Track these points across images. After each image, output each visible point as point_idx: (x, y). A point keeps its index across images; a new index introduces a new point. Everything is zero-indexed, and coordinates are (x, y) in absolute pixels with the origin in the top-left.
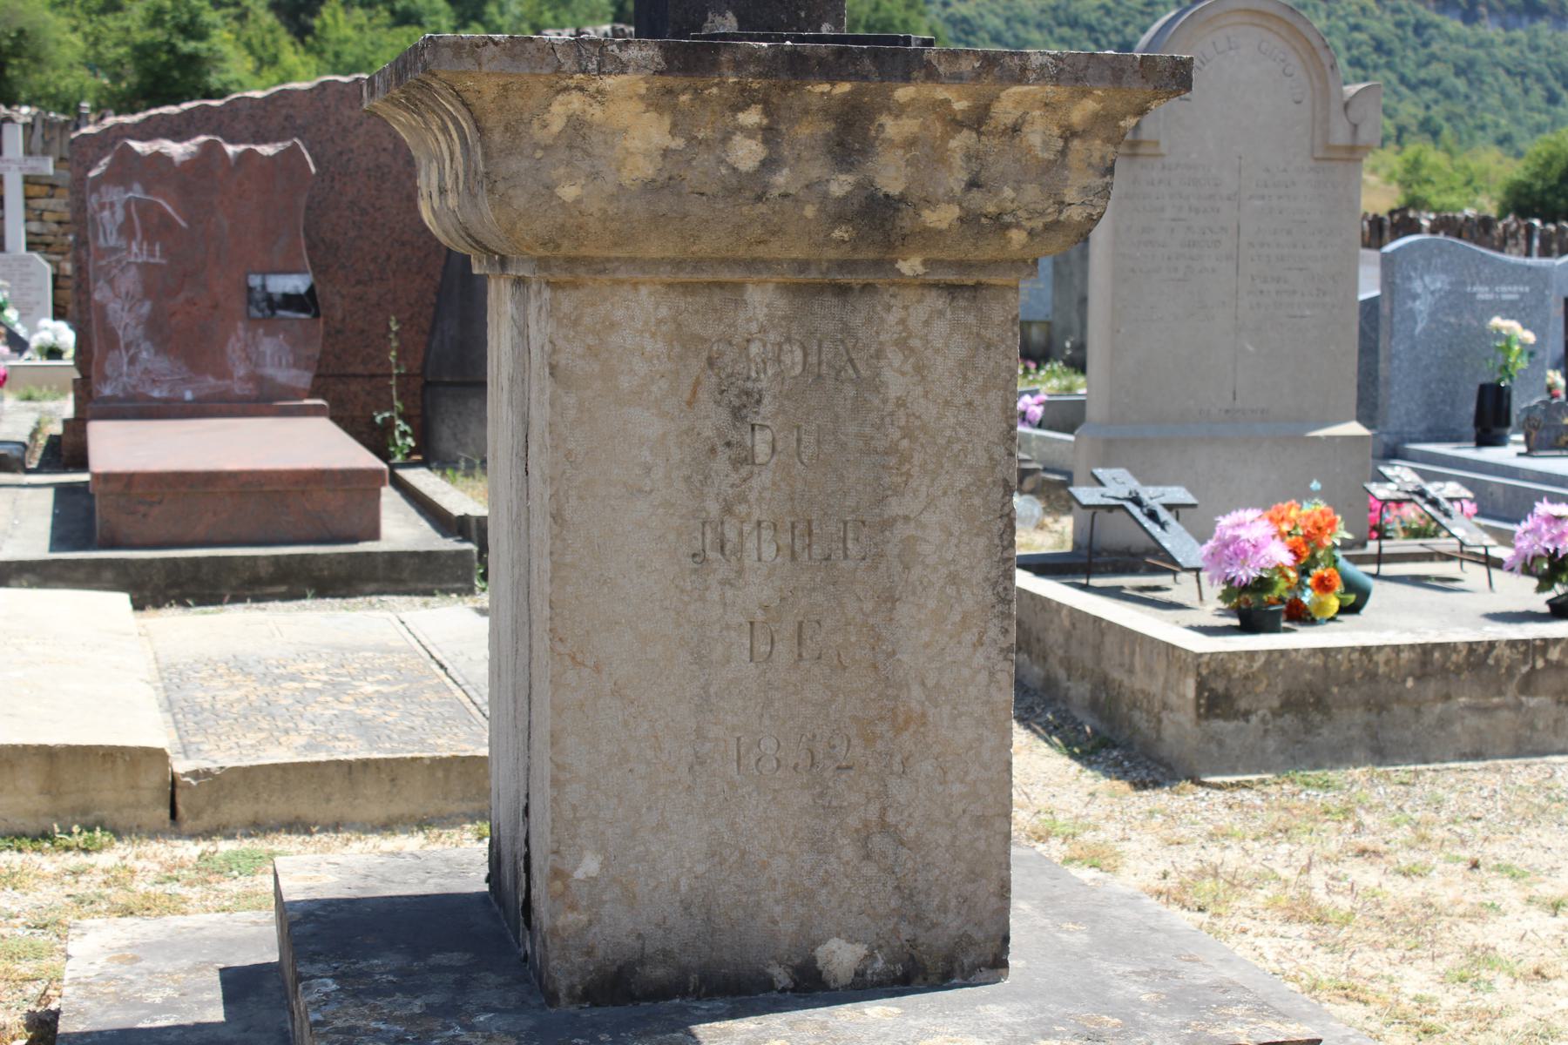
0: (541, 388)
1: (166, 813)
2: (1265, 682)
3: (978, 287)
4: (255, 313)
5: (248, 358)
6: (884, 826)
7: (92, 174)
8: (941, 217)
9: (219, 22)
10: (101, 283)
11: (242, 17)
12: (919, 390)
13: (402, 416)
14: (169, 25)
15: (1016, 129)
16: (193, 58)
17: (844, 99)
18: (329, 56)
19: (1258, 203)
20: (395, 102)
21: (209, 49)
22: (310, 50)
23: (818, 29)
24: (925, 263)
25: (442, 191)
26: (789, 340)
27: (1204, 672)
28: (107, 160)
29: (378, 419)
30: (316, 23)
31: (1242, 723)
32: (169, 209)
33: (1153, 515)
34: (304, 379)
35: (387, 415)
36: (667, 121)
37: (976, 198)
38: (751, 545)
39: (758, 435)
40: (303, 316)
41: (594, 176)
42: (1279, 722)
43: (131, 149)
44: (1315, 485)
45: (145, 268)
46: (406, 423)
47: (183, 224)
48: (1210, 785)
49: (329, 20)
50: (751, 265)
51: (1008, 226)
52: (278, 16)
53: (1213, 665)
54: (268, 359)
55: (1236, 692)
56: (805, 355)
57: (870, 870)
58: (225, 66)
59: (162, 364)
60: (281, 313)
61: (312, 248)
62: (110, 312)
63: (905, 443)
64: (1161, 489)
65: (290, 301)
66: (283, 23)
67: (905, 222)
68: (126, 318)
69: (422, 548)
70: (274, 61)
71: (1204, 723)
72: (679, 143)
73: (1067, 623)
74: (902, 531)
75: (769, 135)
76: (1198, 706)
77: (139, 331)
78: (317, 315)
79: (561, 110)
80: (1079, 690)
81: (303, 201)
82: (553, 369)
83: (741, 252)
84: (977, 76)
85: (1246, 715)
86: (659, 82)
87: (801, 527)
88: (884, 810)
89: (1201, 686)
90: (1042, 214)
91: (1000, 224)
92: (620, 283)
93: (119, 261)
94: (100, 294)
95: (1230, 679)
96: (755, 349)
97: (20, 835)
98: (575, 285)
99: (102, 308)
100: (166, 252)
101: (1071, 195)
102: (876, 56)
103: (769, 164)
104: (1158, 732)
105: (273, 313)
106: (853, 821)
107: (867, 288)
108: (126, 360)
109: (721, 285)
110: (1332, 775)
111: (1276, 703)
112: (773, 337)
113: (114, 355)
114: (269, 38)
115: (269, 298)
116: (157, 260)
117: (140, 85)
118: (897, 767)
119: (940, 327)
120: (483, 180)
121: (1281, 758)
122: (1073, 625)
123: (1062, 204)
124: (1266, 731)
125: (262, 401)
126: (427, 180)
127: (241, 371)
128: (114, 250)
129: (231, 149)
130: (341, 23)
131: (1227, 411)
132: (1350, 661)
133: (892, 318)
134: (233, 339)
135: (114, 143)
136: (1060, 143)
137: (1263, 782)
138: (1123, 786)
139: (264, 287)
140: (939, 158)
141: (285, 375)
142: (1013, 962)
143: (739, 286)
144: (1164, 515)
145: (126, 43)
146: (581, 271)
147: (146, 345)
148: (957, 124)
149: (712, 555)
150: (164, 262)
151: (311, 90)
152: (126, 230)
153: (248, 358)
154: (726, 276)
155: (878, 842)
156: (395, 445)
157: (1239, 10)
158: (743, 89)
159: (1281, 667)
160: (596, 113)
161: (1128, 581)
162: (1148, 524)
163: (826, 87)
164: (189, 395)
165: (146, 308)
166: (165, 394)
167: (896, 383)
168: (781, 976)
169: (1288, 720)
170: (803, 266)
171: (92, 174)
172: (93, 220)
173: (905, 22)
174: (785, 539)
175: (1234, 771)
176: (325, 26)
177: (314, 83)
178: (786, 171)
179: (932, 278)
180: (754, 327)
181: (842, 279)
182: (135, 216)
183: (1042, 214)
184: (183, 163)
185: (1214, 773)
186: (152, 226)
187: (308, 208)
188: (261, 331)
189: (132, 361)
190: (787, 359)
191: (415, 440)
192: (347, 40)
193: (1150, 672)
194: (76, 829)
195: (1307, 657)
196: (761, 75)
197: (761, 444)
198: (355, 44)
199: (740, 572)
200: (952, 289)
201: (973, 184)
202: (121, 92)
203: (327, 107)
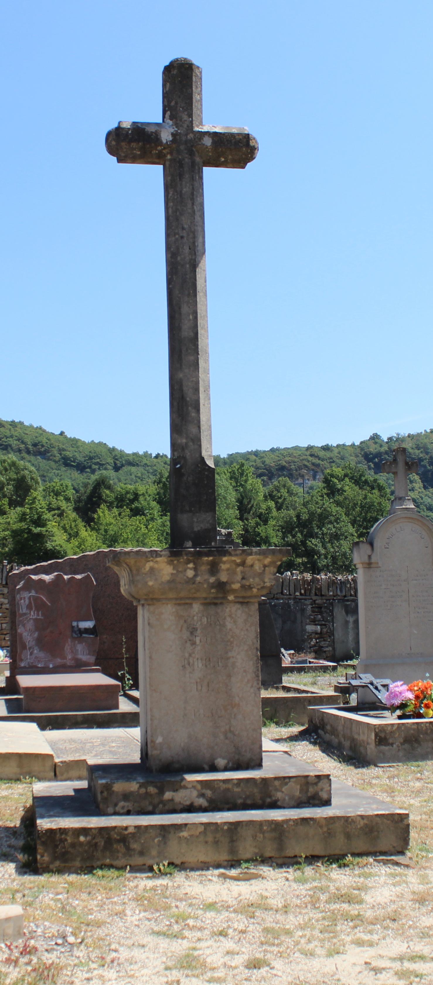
0: (147, 627)
1: (53, 774)
2: (398, 734)
3: (248, 602)
4: (75, 635)
5: (72, 652)
6: (230, 731)
7: (17, 587)
8: (236, 586)
9: (51, 518)
10: (20, 626)
11: (61, 515)
12: (235, 627)
13: (128, 673)
14: (28, 520)
15: (252, 566)
16: (40, 536)
17: (211, 561)
18: (102, 531)
19: (415, 582)
20: (112, 564)
21: (47, 531)
22: (93, 529)
23: (211, 544)
24: (235, 597)
25: (125, 585)
26: (203, 616)
27: (377, 730)
28: (22, 582)
29: (119, 674)
30: (96, 516)
31: (391, 747)
32: (44, 599)
33: (376, 688)
34: (92, 659)
35: (122, 672)
36: (172, 567)
37: (244, 582)
38: (196, 663)
39: (197, 638)
40: (91, 636)
41: (156, 580)
42: (403, 747)
43: (31, 578)
44: (427, 675)
45: (36, 620)
46: (129, 675)
47: (49, 604)
48: (380, 767)
49: (101, 514)
50: (194, 599)
51: (252, 588)
52: (78, 514)
53: (380, 728)
54: (79, 652)
55: (388, 737)
56: (207, 619)
57: (227, 741)
58: (54, 538)
59: (42, 655)
60: (84, 635)
61: (95, 612)
62: (24, 636)
63: (232, 639)
64: (382, 680)
65: (87, 631)
66: (80, 517)
67: (228, 587)
68: (29, 638)
69: (133, 711)
70: (77, 535)
71: (378, 747)
72: (175, 572)
73: (343, 722)
74: (232, 660)
75: (195, 569)
76: (376, 741)
77: (34, 643)
78: (97, 636)
79: (148, 565)
80: (347, 744)
81: (91, 595)
82: (149, 624)
83: (191, 596)
84: (241, 554)
85: (392, 744)
86: (169, 559)
87: (208, 659)
88: (230, 727)
89: (376, 735)
90: (260, 585)
91: (250, 587)
92: (164, 604)
93: (27, 618)
94: (20, 630)
95: (386, 733)
96: (195, 618)
97: (11, 779)
98: (153, 604)
99: (21, 635)
100: (42, 615)
101: (266, 580)
102: (217, 551)
103: (196, 576)
104: (366, 753)
105: (81, 635)
106: (223, 730)
107: (221, 603)
108: (29, 653)
109: (187, 604)
110: (420, 763)
111: (402, 740)
112: (200, 615)
113: (25, 652)
114: (73, 524)
115: (80, 630)
116: (40, 617)
117: (14, 549)
118: (233, 716)
119: (239, 612)
120: (132, 582)
121: (404, 758)
122: (345, 723)
123: (264, 582)
124: (399, 750)
125: (78, 667)
126: (122, 583)
127: (69, 657)
128: (25, 614)
129: (66, 577)
130: (107, 516)
131: (408, 654)
132: (426, 726)
133: (227, 610)
134: (67, 645)
135: (24, 577)
136: (263, 569)
137: (398, 765)
138: (352, 768)
139: (78, 626)
140: (234, 573)
141: (85, 658)
142: (263, 764)
143: (191, 604)
144: (380, 688)
145: (8, 530)
146: (155, 601)
147: (36, 648)
148: (238, 565)
149: (187, 666)
150: (42, 618)
151: (94, 555)
152: (29, 607)
153: (72, 652)
154: (187, 601)
155: (229, 735)
156: (125, 683)
157: (403, 518)
158: (188, 559)
159: (403, 729)
160: (156, 566)
161: (372, 713)
162: (374, 691)
163: (206, 558)
164: (51, 666)
165: (36, 635)
166: (42, 666)
167: (229, 624)
168: (206, 767)
169: (406, 746)
170: (205, 598)
171: (17, 587)
172: (18, 604)
173: (380, 504)
174: (204, 662)
175: (388, 762)
176: (99, 517)
177: (95, 552)
178: (199, 577)
179: (237, 600)
180: (195, 613)
181: (216, 601)
182: (32, 602)
183: (260, 585)
184: (49, 582)
185: (382, 763)
186: (38, 605)
187: (93, 597)
188: (76, 642)
189: (31, 654)
190: (203, 620)
191: (133, 681)
192: (111, 524)
193: (363, 733)
194: (27, 777)
195: (411, 726)
196: (191, 557)
197: (198, 640)
198: (115, 525)
199: (193, 670)
200: (242, 603)
201: (243, 578)
202: (6, 553)
203: (100, 561)
